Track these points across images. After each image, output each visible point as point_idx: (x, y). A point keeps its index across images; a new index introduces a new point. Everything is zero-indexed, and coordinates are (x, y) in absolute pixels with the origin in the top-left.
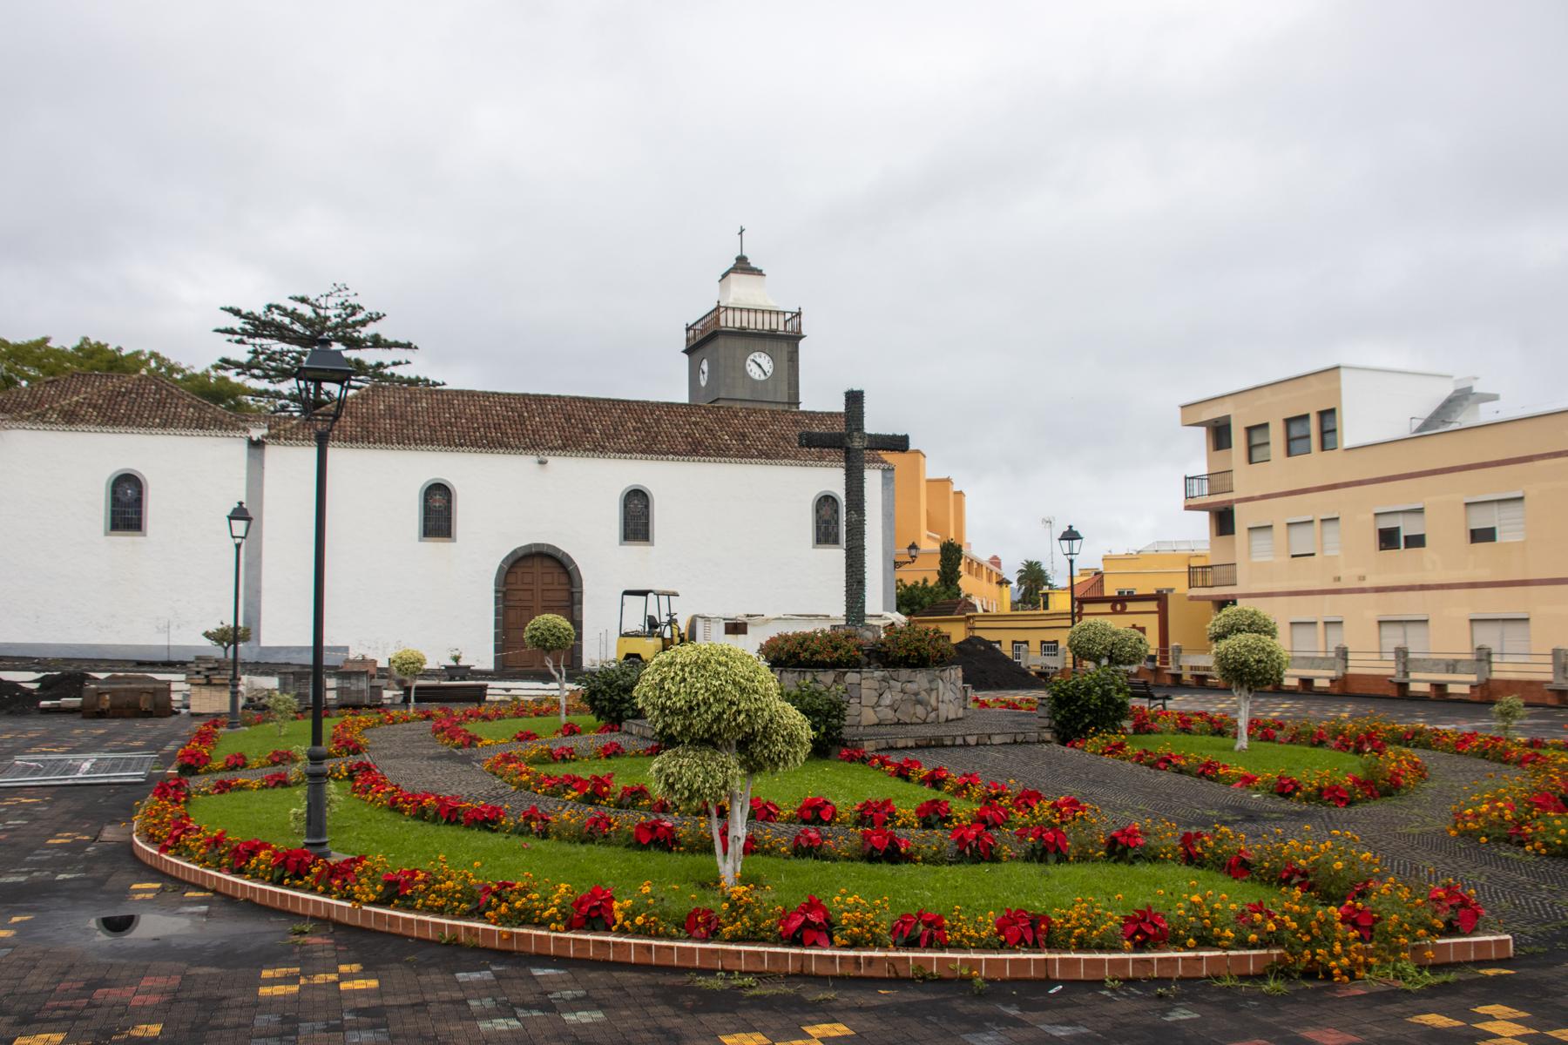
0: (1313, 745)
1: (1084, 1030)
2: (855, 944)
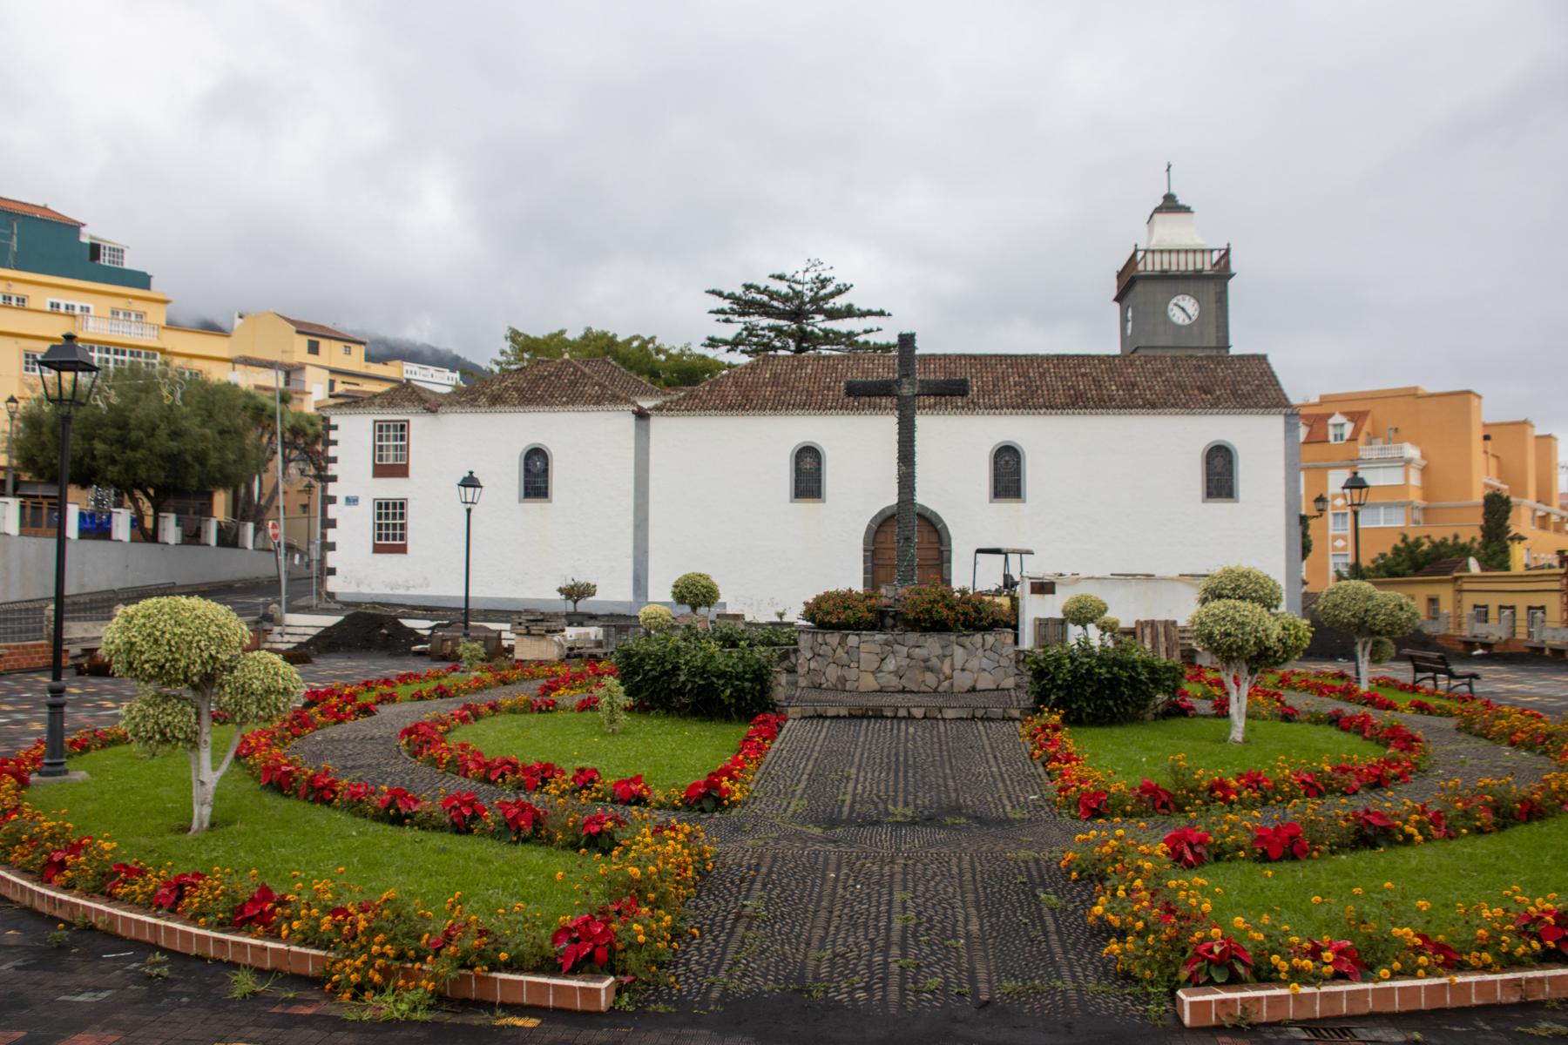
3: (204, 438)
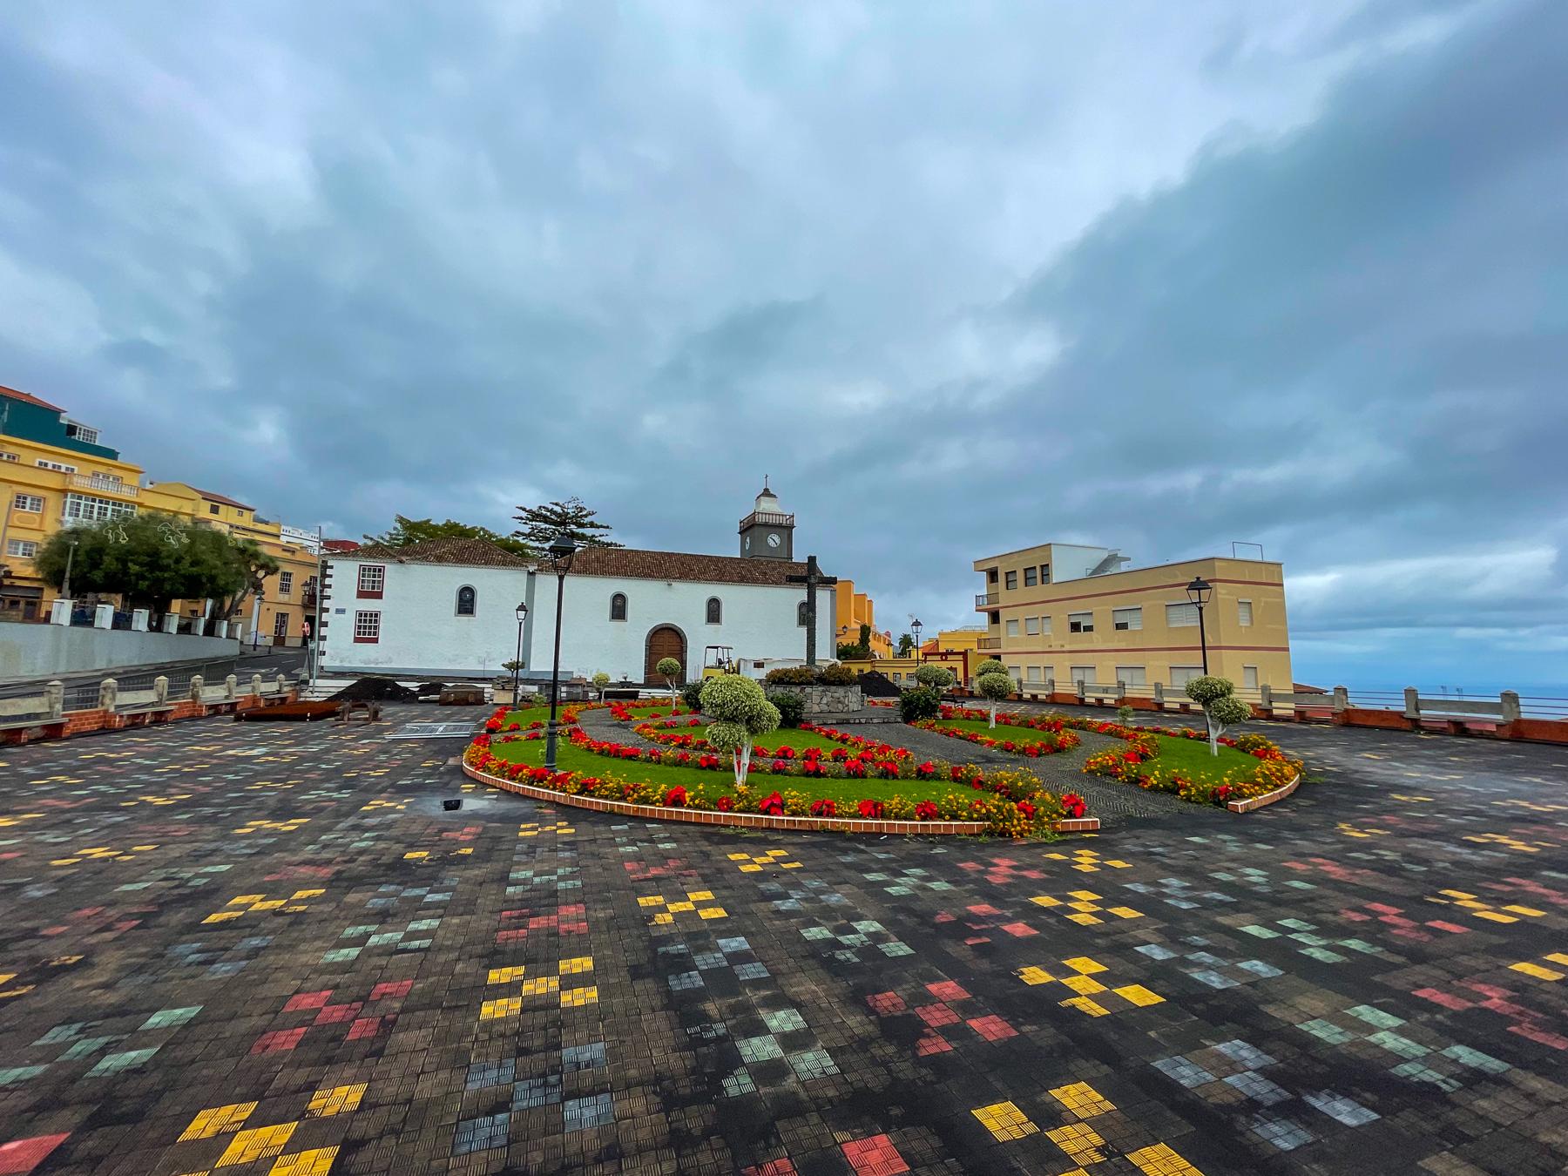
2: (794, 814)
3: (216, 567)
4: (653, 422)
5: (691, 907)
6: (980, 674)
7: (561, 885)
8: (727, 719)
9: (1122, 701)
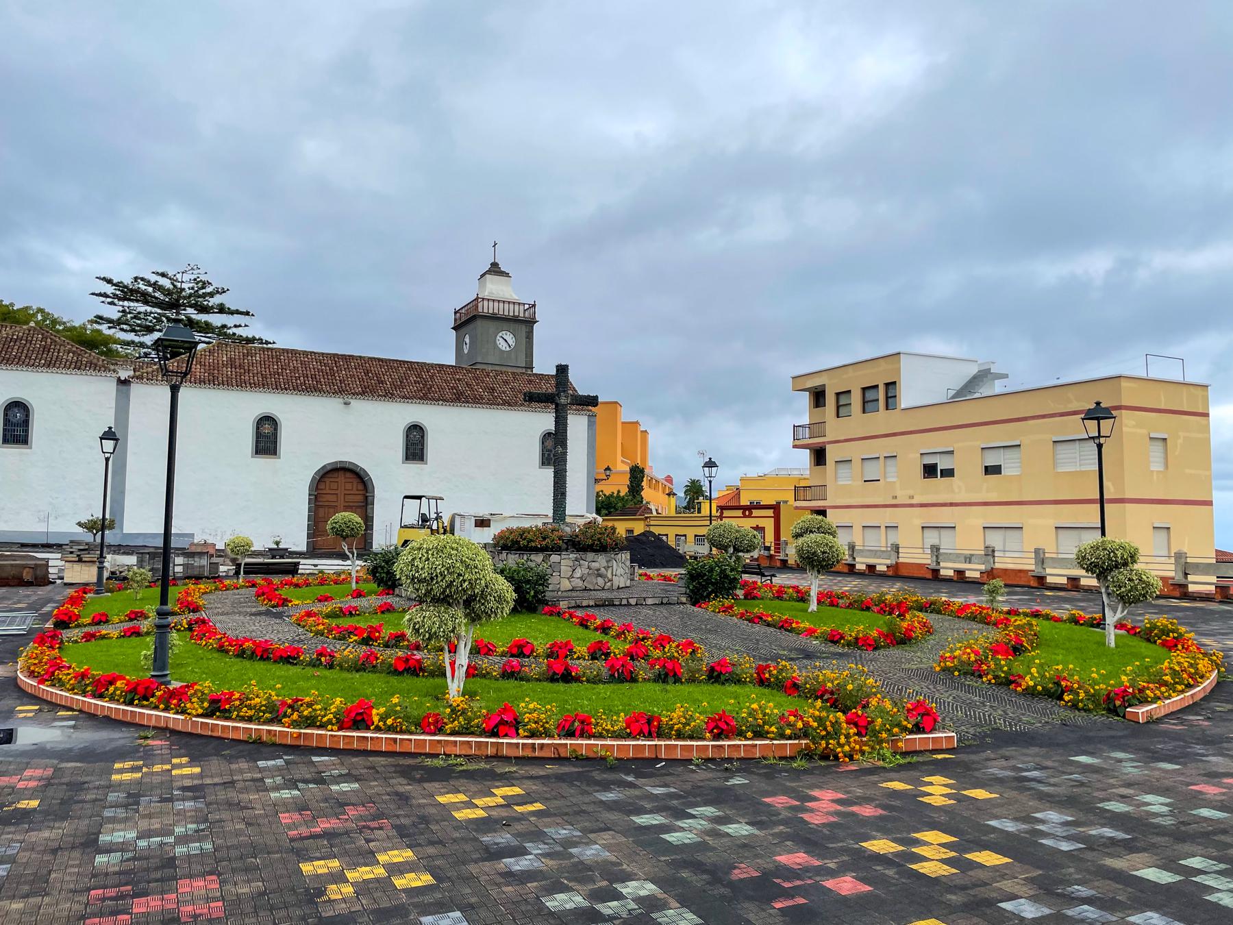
0: (862, 610)
1: (673, 790)
2: (533, 735)
4: (316, 152)
5: (380, 872)
6: (797, 536)
7: (180, 850)
8: (437, 601)
9: (991, 574)
